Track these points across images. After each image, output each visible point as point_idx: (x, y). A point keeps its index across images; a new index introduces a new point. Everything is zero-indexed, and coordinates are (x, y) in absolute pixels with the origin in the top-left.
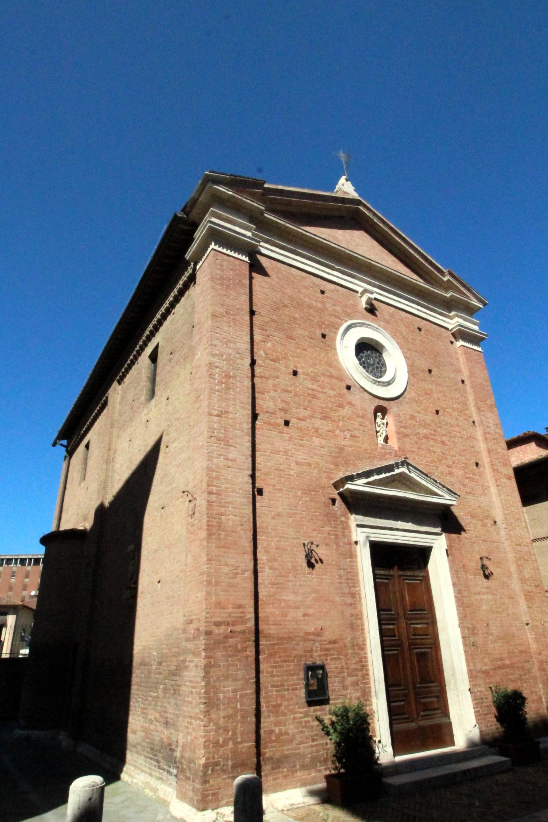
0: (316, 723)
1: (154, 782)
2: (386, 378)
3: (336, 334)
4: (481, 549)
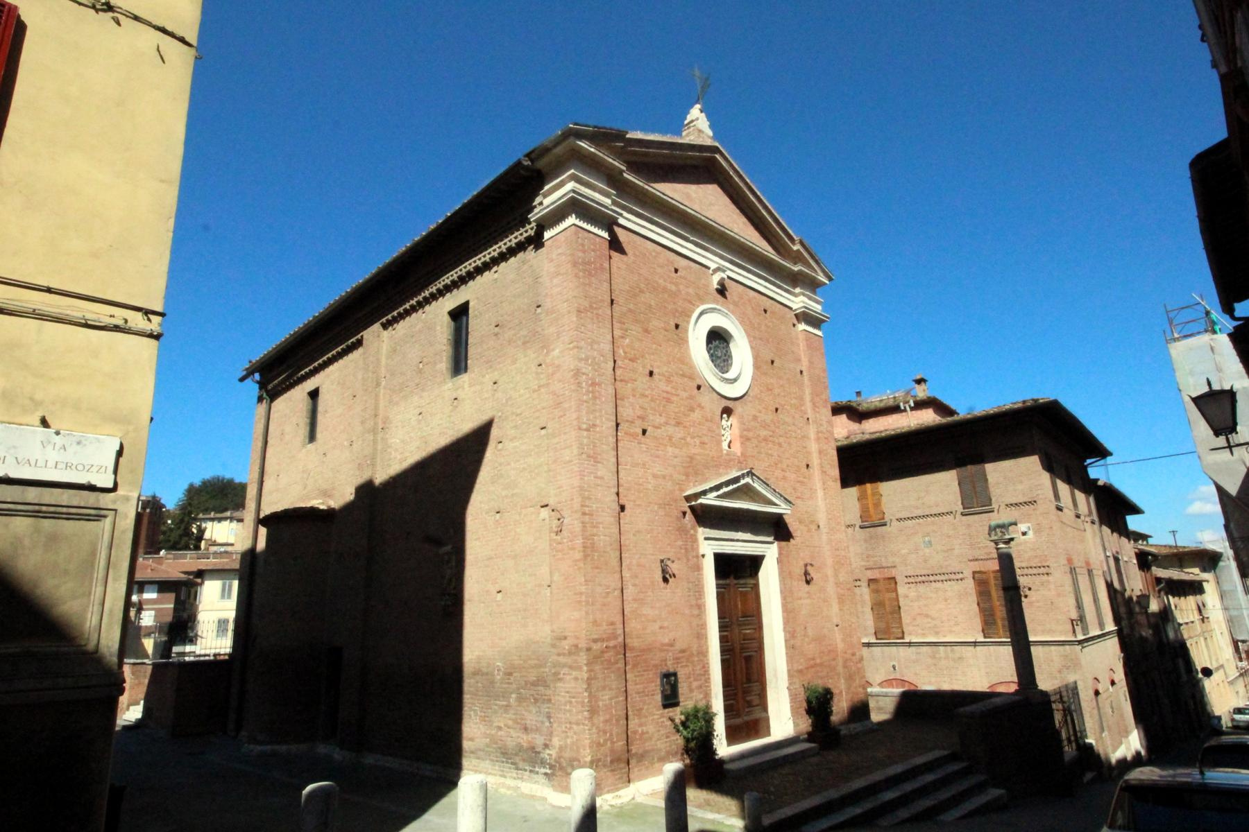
0: (669, 723)
1: (509, 782)
2: (730, 375)
3: (688, 322)
4: (805, 556)
